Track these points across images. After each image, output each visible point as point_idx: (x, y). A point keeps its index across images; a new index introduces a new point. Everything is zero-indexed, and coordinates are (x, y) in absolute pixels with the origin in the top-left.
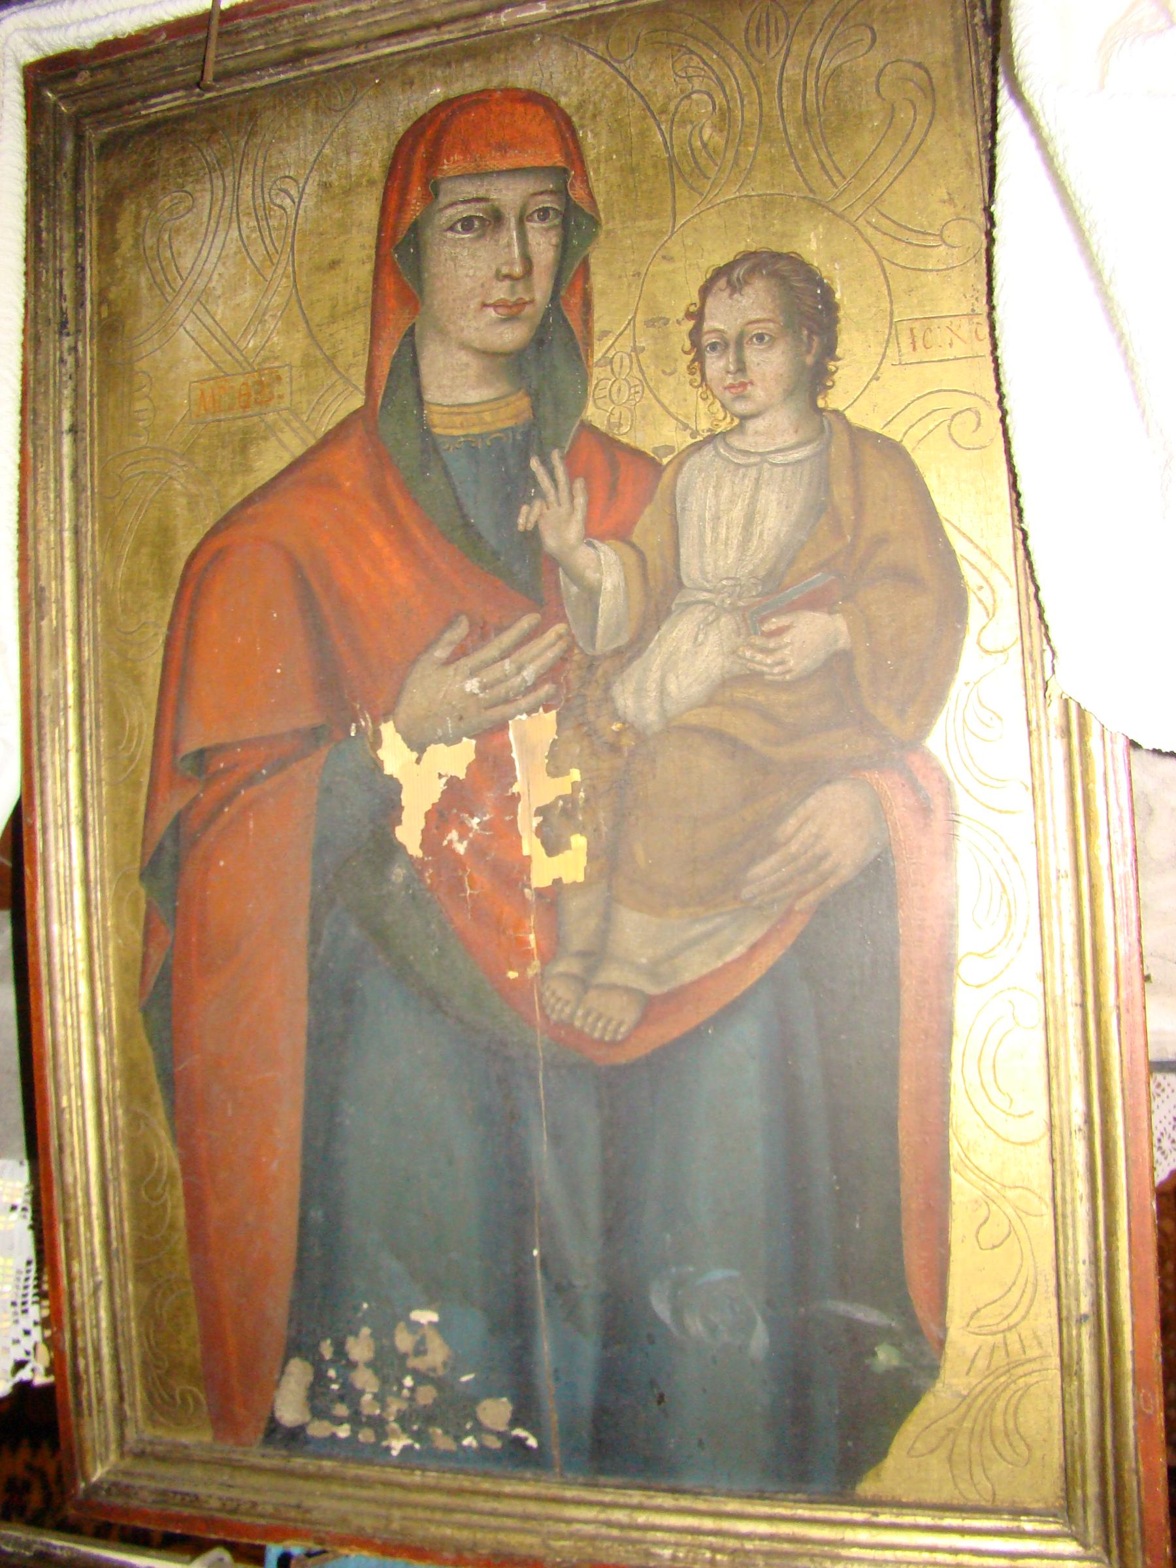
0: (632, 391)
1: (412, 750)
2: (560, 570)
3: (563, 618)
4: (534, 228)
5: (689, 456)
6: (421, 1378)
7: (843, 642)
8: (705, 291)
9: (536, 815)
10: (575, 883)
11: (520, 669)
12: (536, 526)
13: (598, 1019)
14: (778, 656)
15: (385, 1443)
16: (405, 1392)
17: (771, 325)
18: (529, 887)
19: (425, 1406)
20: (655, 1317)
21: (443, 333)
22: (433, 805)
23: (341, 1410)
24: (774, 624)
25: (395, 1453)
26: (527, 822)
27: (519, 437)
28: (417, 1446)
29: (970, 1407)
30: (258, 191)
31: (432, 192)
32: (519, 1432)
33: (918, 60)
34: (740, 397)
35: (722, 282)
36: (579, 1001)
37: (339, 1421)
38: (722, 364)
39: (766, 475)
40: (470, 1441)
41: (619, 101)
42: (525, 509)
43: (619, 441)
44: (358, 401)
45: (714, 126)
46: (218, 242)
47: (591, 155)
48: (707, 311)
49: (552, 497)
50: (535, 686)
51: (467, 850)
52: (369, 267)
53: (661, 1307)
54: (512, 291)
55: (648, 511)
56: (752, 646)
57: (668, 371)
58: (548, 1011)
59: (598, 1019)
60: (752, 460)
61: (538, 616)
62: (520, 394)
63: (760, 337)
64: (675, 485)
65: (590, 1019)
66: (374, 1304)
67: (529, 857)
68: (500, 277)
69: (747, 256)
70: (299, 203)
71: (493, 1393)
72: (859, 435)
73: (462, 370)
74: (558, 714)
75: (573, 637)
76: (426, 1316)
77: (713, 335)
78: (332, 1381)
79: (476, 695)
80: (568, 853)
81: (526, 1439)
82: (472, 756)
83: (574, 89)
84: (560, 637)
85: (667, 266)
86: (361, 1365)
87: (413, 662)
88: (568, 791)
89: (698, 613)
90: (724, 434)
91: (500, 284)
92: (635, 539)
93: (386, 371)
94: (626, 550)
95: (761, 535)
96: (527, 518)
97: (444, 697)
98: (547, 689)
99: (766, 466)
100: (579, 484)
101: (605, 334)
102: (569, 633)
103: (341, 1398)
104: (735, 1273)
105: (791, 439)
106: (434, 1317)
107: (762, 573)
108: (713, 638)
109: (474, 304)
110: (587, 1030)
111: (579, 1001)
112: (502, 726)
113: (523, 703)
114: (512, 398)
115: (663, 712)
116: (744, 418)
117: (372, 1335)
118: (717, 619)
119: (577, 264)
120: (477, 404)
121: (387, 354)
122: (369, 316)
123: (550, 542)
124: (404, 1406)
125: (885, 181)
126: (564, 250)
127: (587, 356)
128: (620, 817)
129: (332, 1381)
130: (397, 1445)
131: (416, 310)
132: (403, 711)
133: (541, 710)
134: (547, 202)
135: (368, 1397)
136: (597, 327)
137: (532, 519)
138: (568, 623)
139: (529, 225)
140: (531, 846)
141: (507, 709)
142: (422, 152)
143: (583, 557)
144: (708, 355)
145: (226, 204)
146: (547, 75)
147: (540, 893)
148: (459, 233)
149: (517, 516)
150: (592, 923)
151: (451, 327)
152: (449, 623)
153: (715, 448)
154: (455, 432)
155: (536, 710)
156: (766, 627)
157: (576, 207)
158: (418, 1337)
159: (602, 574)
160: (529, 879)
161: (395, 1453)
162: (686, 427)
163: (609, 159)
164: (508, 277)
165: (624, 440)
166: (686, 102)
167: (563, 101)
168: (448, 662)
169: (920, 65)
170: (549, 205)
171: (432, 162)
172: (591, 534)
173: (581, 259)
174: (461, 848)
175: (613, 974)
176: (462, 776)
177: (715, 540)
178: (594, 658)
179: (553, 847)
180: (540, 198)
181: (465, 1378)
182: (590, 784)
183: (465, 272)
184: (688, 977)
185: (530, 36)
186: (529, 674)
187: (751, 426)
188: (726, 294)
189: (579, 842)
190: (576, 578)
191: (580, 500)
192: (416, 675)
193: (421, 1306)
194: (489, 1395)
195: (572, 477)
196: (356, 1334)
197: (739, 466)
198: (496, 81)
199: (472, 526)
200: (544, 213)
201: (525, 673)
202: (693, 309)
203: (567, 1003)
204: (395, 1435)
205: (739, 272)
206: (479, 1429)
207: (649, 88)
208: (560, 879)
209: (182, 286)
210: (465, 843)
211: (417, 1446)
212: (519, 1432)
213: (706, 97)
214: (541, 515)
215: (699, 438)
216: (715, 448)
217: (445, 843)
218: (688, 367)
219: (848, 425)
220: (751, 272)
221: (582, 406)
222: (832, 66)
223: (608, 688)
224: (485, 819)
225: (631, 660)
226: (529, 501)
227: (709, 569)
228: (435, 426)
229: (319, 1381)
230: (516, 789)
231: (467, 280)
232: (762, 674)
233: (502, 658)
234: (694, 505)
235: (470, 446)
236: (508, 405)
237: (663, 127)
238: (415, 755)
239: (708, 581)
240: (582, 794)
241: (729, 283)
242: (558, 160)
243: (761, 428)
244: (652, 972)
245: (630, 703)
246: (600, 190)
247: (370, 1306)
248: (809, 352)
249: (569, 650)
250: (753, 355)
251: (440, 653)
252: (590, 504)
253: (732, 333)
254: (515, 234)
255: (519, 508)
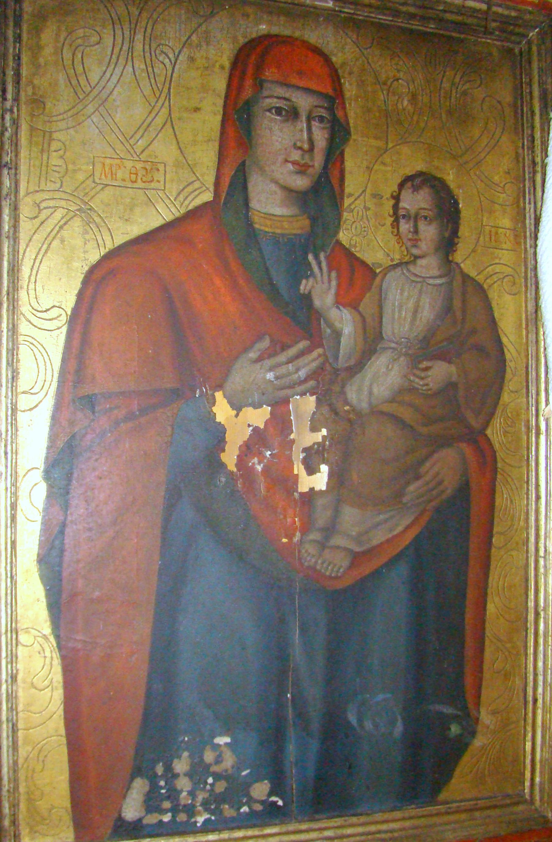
0: (363, 230)
1: (233, 409)
2: (322, 319)
3: (321, 345)
4: (315, 124)
5: (389, 271)
6: (217, 777)
7: (454, 378)
8: (401, 186)
9: (302, 452)
10: (321, 490)
11: (298, 370)
12: (310, 292)
13: (329, 565)
14: (426, 381)
15: (193, 820)
16: (208, 787)
17: (430, 213)
18: (297, 491)
19: (220, 793)
20: (349, 723)
21: (262, 170)
22: (244, 441)
23: (167, 805)
24: (425, 364)
25: (198, 825)
26: (298, 456)
27: (303, 241)
28: (213, 818)
29: (486, 750)
30: (147, 47)
31: (259, 86)
32: (274, 799)
33: (499, 100)
34: (415, 246)
35: (409, 184)
36: (320, 555)
37: (163, 811)
38: (407, 226)
39: (424, 288)
40: (245, 809)
41: (363, 70)
42: (304, 282)
43: (355, 255)
44: (208, 197)
45: (409, 101)
46: (118, 71)
47: (347, 95)
48: (401, 197)
49: (319, 279)
50: (305, 380)
51: (263, 469)
52: (219, 118)
53: (352, 719)
54: (303, 156)
55: (368, 295)
56: (414, 375)
57: (381, 224)
58: (303, 561)
59: (329, 565)
60: (419, 280)
61: (308, 342)
62: (305, 216)
63: (425, 218)
64: (381, 286)
65: (325, 565)
66: (190, 737)
67: (297, 475)
68: (296, 147)
69: (421, 174)
70: (175, 63)
71: (259, 779)
72: (466, 277)
73: (272, 194)
74: (317, 398)
75: (327, 357)
76: (223, 740)
77: (404, 211)
78: (162, 788)
79: (273, 381)
80: (318, 474)
81: (277, 801)
82: (268, 416)
83: (340, 54)
84: (320, 356)
85: (382, 168)
86: (181, 775)
87: (237, 357)
88: (320, 440)
89: (389, 353)
90: (407, 263)
91: (296, 151)
92: (361, 309)
93: (227, 184)
94: (356, 314)
95: (421, 319)
96: (305, 287)
97: (254, 380)
98: (312, 383)
99: (425, 284)
100: (334, 274)
101: (350, 195)
102: (325, 354)
103: (168, 798)
104: (389, 695)
105: (436, 272)
106: (228, 740)
107: (421, 338)
108: (396, 367)
109: (281, 158)
110: (323, 571)
111: (320, 555)
112: (286, 401)
113: (299, 389)
114: (301, 218)
115: (370, 403)
116: (416, 257)
117: (190, 756)
118: (399, 358)
119: (338, 152)
120: (280, 216)
121: (229, 172)
122: (217, 147)
123: (317, 303)
124: (206, 795)
125: (483, 155)
126: (331, 141)
127: (341, 205)
128: (346, 456)
129: (162, 788)
130: (200, 820)
131: (246, 152)
132: (229, 386)
133: (308, 394)
134: (323, 113)
135: (184, 794)
136: (347, 190)
137: (308, 288)
138: (324, 348)
139: (313, 123)
140: (299, 469)
141: (289, 392)
142: (253, 59)
143: (334, 314)
144: (401, 220)
145: (124, 48)
146: (326, 42)
147: (302, 494)
148: (272, 114)
149: (300, 284)
150: (329, 513)
151: (267, 169)
152: (259, 338)
153: (402, 270)
154: (267, 230)
155: (305, 394)
156: (421, 366)
157: (338, 120)
158: (218, 753)
159: (343, 324)
160: (297, 487)
161: (198, 825)
162: (388, 255)
163: (356, 100)
164: (300, 148)
165: (358, 255)
166: (395, 83)
167: (334, 59)
168: (259, 360)
169: (499, 102)
170: (324, 115)
171: (259, 68)
172: (339, 303)
173: (340, 150)
174: (259, 468)
175: (338, 541)
176: (262, 427)
177: (400, 317)
178: (338, 370)
179: (311, 470)
180: (319, 109)
181: (244, 773)
182: (330, 437)
183: (277, 138)
184: (375, 542)
185: (318, 16)
186: (302, 374)
187: (419, 262)
188: (410, 191)
189: (324, 468)
190: (330, 325)
191: (334, 283)
192: (237, 365)
193: (221, 735)
194: (257, 781)
195: (330, 270)
196: (179, 757)
197: (413, 281)
198: (297, 34)
199: (275, 284)
200: (321, 119)
201: (300, 373)
202: (395, 194)
203: (313, 556)
204: (200, 814)
205: (417, 181)
206: (251, 801)
207: (378, 69)
208: (314, 488)
209: (91, 92)
210: (262, 465)
211: (213, 818)
212: (274, 799)
213: (405, 84)
214: (313, 287)
215: (395, 263)
216: (402, 270)
217: (250, 464)
218: (391, 224)
219: (462, 272)
220: (423, 183)
221: (336, 232)
222: (463, 89)
223: (343, 387)
224: (274, 452)
225: (356, 373)
226: (307, 278)
227: (396, 331)
228: (256, 223)
229: (154, 787)
230: (292, 436)
231: (277, 143)
232: (417, 389)
233: (287, 363)
234: (390, 296)
235: (276, 240)
236: (297, 221)
237: (385, 92)
238: (234, 412)
239: (395, 338)
240: (327, 443)
241: (413, 185)
242: (330, 92)
243: (423, 265)
244: (358, 540)
245: (354, 396)
246: (351, 115)
247: (188, 739)
248: (447, 230)
249: (324, 364)
250: (422, 226)
251: (253, 355)
252: (339, 286)
253: (413, 212)
254: (305, 125)
255: (301, 281)
